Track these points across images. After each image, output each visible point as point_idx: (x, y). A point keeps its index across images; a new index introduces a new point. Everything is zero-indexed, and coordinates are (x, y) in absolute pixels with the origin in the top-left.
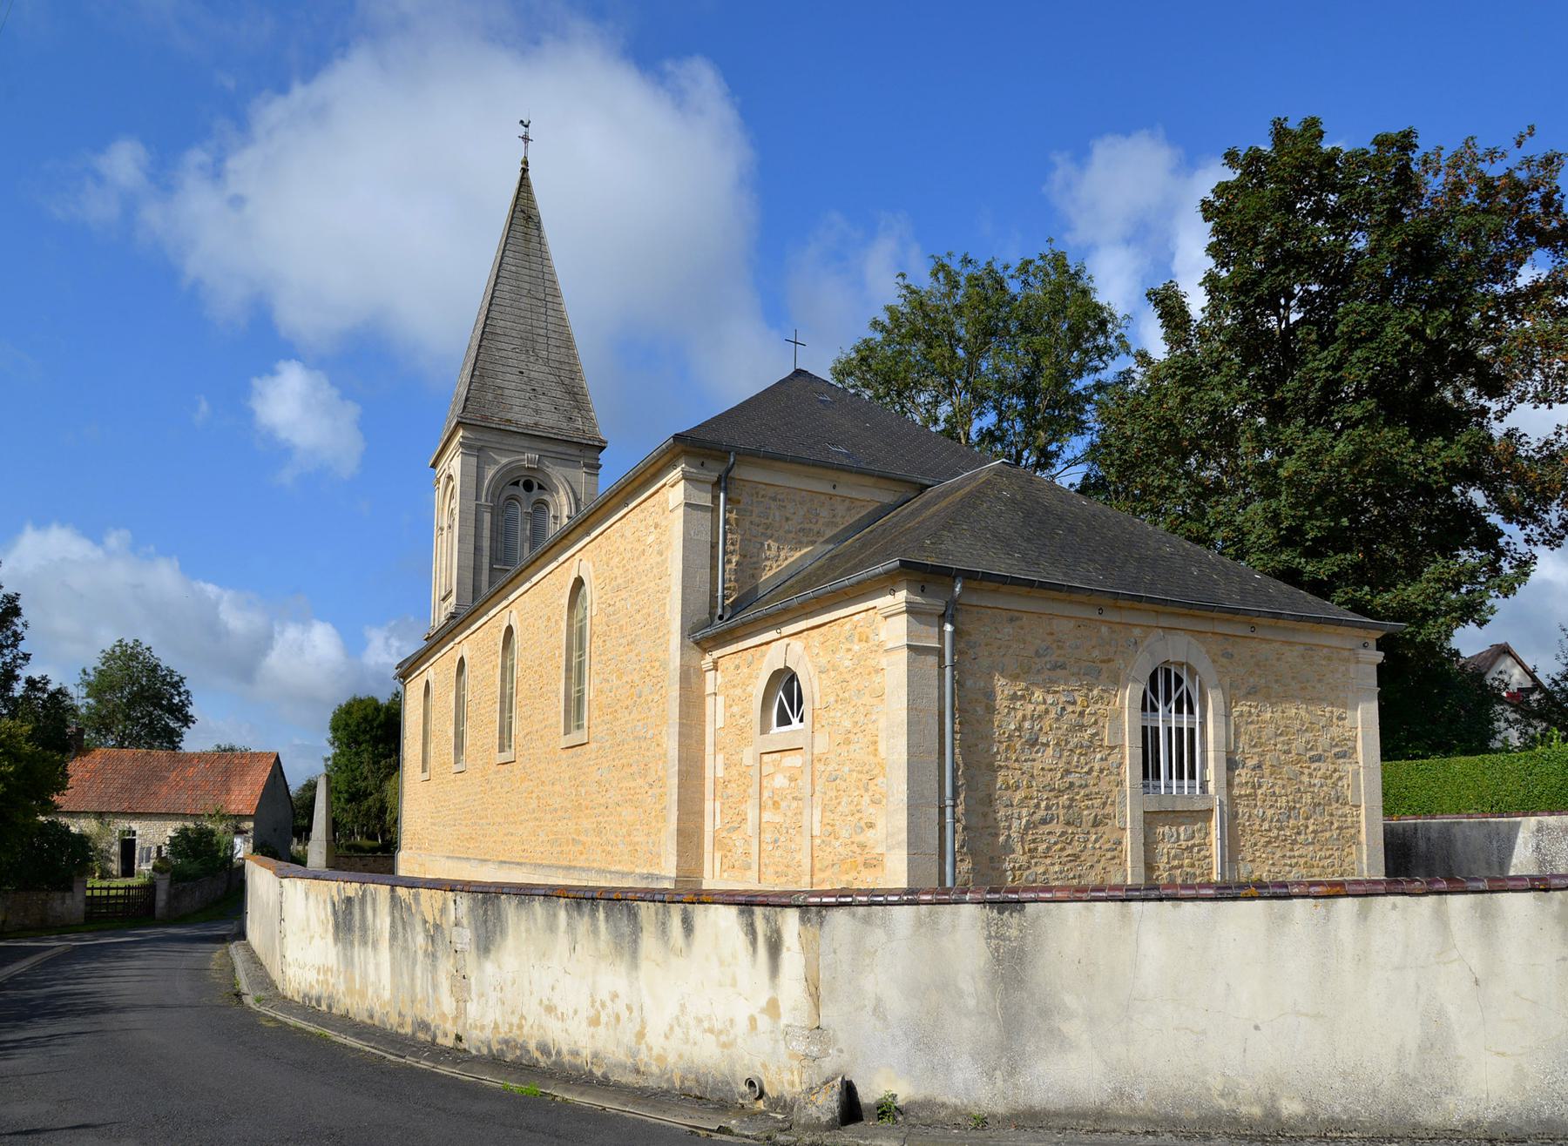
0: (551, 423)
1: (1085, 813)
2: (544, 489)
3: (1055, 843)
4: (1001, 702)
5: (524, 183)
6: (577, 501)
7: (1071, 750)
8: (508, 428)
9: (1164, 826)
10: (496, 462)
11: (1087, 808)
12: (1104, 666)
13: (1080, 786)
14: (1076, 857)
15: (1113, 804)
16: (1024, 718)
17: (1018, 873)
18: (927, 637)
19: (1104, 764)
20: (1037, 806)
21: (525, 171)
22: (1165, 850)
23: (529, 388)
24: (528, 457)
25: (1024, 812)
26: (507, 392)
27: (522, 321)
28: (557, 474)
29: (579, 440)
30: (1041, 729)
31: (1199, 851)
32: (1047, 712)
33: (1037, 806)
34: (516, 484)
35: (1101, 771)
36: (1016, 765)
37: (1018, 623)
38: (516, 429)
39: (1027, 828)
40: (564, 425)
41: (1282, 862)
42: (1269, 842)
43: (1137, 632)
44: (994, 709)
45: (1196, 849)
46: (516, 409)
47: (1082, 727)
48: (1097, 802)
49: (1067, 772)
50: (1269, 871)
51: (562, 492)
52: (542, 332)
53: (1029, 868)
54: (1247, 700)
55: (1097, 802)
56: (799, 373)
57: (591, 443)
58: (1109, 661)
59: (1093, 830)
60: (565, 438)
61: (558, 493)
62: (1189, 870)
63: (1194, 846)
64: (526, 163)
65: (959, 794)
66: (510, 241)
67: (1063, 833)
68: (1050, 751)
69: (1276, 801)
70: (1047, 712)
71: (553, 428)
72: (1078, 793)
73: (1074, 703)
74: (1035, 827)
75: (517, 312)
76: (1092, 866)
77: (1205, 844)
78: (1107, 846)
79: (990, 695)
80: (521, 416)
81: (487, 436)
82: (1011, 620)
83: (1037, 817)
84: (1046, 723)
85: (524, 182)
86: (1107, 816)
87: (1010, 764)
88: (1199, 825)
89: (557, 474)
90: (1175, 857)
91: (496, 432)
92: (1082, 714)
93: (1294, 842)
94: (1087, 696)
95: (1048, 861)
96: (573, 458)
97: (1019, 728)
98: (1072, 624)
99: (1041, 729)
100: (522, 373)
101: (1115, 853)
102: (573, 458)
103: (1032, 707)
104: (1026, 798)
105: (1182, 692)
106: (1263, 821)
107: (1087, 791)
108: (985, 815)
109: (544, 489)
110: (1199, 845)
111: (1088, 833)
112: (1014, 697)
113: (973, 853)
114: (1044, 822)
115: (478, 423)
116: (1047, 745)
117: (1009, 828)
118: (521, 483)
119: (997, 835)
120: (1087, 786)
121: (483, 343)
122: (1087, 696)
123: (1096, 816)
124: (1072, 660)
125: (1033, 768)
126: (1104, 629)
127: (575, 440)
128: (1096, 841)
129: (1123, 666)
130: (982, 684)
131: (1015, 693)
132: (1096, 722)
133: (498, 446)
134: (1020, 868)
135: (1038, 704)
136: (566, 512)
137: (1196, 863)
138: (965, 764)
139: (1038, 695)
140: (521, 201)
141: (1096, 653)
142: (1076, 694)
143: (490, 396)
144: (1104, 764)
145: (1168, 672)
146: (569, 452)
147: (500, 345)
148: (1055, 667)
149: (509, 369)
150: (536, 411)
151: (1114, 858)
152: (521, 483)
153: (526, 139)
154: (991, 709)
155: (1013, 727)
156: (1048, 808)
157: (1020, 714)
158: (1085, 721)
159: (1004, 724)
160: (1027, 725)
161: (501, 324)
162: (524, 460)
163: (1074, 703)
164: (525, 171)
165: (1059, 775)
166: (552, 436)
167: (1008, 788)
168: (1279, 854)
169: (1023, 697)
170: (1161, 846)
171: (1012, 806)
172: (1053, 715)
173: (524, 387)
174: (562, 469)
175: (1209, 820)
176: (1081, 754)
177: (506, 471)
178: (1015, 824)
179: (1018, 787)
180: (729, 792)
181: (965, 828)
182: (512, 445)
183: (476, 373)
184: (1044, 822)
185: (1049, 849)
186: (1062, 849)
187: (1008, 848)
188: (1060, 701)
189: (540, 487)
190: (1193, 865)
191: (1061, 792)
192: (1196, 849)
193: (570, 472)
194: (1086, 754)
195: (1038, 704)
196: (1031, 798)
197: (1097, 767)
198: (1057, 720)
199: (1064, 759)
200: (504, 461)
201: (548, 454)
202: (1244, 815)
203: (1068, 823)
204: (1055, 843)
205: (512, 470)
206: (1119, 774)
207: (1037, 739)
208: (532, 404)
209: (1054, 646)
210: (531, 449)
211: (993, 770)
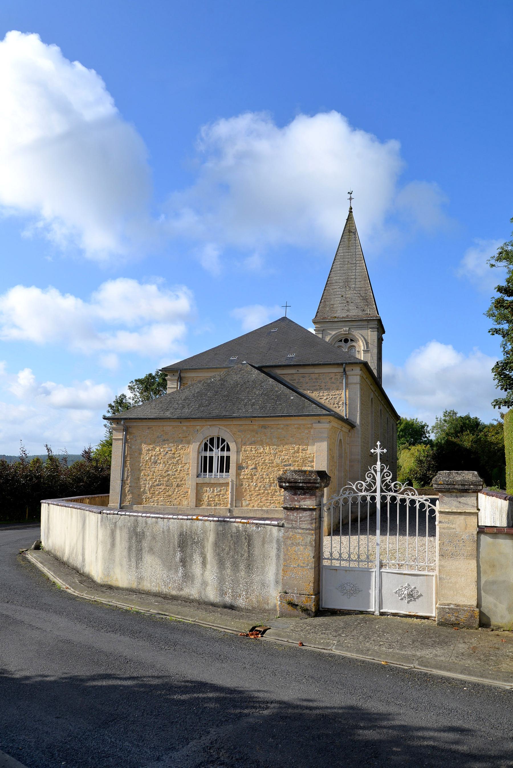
0: (354, 314)
1: (174, 483)
2: (353, 341)
3: (162, 492)
4: (144, 451)
5: (350, 218)
6: (367, 343)
7: (169, 465)
8: (334, 320)
9: (207, 487)
10: (330, 334)
11: (175, 481)
12: (184, 439)
13: (172, 475)
14: (170, 496)
15: (185, 480)
16: (152, 456)
17: (148, 499)
18: (119, 436)
19: (182, 469)
20: (156, 481)
21: (351, 212)
22: (207, 495)
23: (345, 302)
24: (345, 329)
25: (151, 482)
26: (335, 306)
27: (344, 275)
28: (357, 333)
29: (366, 319)
30: (158, 459)
31: (222, 496)
32: (160, 454)
33: (156, 481)
34: (341, 341)
35: (181, 470)
36: (149, 469)
37: (152, 429)
38: (337, 320)
39: (151, 487)
40: (360, 313)
41: (266, 502)
42: (258, 495)
43: (198, 427)
44: (141, 453)
45: (221, 496)
46: (339, 311)
47: (174, 458)
48: (178, 480)
49: (167, 471)
50: (259, 504)
51: (360, 341)
52: (353, 277)
53: (151, 498)
54: (250, 445)
55: (178, 480)
56: (284, 319)
57: (372, 318)
58: (186, 437)
59: (177, 488)
60: (359, 319)
61: (359, 341)
62: (217, 502)
63: (221, 494)
64: (351, 208)
65: (129, 477)
66: (341, 243)
67: (164, 489)
68: (161, 465)
69: (264, 480)
70: (160, 454)
71: (355, 316)
72: (171, 477)
73: (171, 450)
74: (154, 486)
75: (342, 272)
76: (175, 499)
77: (226, 494)
78: (182, 493)
79: (140, 450)
80: (340, 313)
81: (326, 325)
82: (148, 428)
83: (155, 484)
84: (160, 457)
85: (350, 217)
86: (183, 484)
87: (146, 469)
88: (223, 488)
89: (357, 333)
90: (211, 498)
91: (329, 323)
92: (174, 454)
93: (274, 495)
94: (176, 448)
95: (159, 497)
96: (365, 326)
97: (150, 459)
98: (171, 428)
99: (158, 459)
100: (343, 296)
101: (185, 495)
102: (365, 326)
103: (155, 452)
104: (151, 478)
105: (225, 445)
106: (256, 487)
107: (175, 476)
108: (137, 483)
109: (353, 341)
110: (223, 494)
111: (175, 489)
112: (149, 450)
113: (132, 493)
114: (158, 485)
115: (321, 321)
116: (160, 463)
117: (145, 487)
118: (343, 340)
119: (141, 489)
120: (174, 475)
121: (326, 288)
122: (176, 448)
123: (178, 484)
124: (171, 438)
125: (155, 470)
126: (185, 428)
127: (364, 319)
128: (178, 491)
129: (192, 438)
130: (138, 447)
131: (149, 449)
132: (179, 456)
133: (331, 328)
134: (148, 498)
135: (157, 452)
136: (362, 348)
137: (221, 500)
138: (131, 469)
139: (158, 449)
140: (348, 225)
141: (180, 435)
142: (172, 448)
143: (328, 309)
144: (182, 469)
145: (218, 438)
146: (363, 324)
147: (333, 287)
148: (164, 440)
149: (337, 296)
150: (348, 311)
151: (184, 497)
152: (343, 340)
153: (351, 199)
154: (140, 454)
155: (147, 458)
156: (159, 481)
157: (150, 455)
158: (175, 456)
159: (145, 458)
160: (153, 458)
161: (334, 278)
162: (342, 331)
163: (171, 450)
164: (351, 212)
165: (164, 472)
166: (353, 319)
167: (145, 475)
168: (264, 499)
169: (152, 450)
170: (205, 494)
171: (146, 480)
172: (163, 455)
173: (343, 302)
174: (360, 332)
175: (228, 486)
176: (173, 466)
177: (336, 336)
178: (147, 486)
179: (149, 475)
180: (265, 466)
181: (130, 486)
182: (337, 326)
183: (323, 301)
184: (158, 485)
185: (159, 493)
186: (165, 493)
187: (144, 492)
188: (166, 450)
189: (352, 340)
190: (220, 501)
191: (165, 477)
192: (221, 496)
193: (364, 332)
194: (175, 466)
195: (157, 452)
196: (153, 478)
197: (179, 469)
198: (164, 456)
199: (166, 467)
200: (334, 333)
201: (352, 327)
202: (246, 485)
203: (167, 486)
204: (162, 492)
205: (339, 335)
206: (188, 471)
207: (156, 462)
208: (346, 308)
209: (164, 434)
210: (345, 326)
211: (140, 471)
